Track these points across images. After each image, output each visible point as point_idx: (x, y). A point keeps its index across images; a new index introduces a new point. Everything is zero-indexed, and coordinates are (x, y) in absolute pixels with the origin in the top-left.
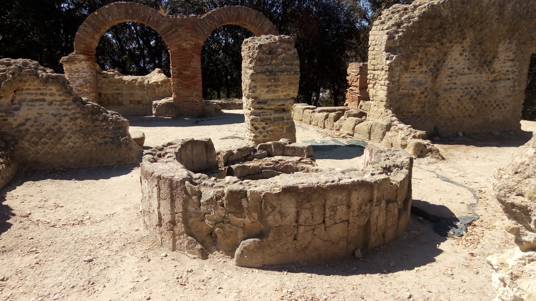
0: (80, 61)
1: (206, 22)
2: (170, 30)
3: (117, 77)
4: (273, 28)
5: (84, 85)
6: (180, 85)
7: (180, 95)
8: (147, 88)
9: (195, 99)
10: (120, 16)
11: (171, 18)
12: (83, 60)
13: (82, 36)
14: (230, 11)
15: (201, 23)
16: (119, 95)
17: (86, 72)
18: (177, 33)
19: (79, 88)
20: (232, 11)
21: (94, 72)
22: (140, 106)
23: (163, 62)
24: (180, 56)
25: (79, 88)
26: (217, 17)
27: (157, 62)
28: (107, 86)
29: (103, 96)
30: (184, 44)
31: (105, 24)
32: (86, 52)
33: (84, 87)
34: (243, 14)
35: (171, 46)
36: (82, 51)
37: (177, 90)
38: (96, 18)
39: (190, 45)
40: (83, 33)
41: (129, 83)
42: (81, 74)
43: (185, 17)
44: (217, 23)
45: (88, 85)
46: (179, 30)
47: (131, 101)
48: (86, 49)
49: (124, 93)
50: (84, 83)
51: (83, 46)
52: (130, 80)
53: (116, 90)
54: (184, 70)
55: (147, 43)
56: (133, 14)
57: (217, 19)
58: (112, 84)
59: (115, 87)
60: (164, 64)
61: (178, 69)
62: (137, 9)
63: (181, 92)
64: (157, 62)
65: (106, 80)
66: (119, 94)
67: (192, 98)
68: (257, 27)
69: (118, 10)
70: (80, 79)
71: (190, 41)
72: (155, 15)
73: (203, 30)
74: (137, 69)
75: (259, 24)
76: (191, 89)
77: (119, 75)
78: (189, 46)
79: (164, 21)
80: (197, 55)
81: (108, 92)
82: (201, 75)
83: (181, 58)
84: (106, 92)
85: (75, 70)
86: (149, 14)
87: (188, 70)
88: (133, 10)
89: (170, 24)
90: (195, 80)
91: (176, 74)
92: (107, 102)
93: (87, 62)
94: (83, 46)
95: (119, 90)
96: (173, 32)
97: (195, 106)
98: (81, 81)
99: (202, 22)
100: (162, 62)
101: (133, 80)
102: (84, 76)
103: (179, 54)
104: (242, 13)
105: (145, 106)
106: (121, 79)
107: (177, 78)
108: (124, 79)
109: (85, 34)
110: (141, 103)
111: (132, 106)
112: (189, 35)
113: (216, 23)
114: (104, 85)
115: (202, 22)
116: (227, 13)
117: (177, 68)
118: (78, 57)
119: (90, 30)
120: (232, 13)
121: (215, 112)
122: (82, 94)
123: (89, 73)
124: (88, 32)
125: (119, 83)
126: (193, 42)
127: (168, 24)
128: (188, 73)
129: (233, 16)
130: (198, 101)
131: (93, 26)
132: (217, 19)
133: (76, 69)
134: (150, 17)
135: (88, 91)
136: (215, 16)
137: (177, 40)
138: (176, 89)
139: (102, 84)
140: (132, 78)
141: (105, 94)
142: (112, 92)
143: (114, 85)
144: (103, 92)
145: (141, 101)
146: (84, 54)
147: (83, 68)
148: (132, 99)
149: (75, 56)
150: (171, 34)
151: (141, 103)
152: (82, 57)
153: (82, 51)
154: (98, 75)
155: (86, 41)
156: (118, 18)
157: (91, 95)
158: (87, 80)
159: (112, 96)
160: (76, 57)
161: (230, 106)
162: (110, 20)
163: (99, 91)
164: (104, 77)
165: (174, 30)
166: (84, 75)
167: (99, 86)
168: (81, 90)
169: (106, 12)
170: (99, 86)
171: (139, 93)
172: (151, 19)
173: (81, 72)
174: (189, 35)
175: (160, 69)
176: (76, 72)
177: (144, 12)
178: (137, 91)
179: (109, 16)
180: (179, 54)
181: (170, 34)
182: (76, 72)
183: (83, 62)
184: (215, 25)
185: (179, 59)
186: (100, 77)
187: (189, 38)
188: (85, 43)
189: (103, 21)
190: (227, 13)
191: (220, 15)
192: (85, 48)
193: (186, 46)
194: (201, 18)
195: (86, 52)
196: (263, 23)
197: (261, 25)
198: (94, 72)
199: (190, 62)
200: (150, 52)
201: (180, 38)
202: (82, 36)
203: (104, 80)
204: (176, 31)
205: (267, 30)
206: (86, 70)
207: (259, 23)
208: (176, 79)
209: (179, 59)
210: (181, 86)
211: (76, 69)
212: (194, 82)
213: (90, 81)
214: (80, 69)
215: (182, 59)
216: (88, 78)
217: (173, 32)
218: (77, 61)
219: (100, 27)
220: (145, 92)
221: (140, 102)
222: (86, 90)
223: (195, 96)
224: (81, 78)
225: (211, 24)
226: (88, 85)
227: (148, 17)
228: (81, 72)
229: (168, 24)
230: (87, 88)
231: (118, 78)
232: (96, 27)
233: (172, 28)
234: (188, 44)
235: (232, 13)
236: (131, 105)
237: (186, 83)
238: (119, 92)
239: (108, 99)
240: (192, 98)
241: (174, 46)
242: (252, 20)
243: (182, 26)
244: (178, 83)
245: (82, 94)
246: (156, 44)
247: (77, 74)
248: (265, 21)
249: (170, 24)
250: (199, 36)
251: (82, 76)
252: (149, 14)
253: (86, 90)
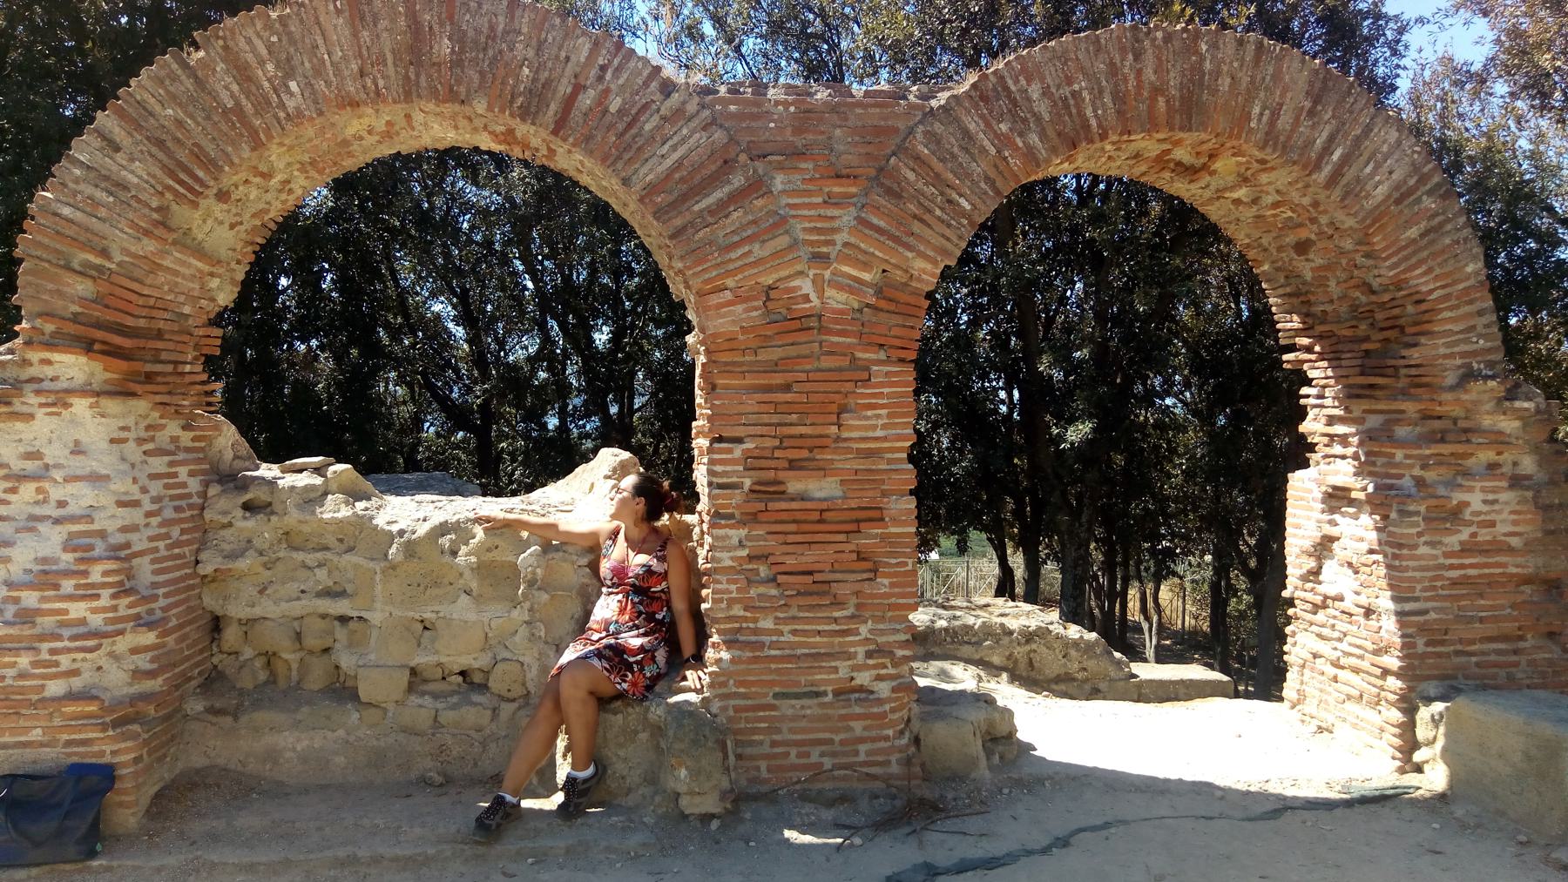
0: (60, 399)
1: (966, 133)
2: (714, 180)
3: (335, 509)
4: (1423, 179)
5: (68, 574)
6: (764, 571)
7: (762, 645)
8: (531, 583)
9: (863, 678)
10: (362, 74)
11: (723, 101)
12: (84, 392)
13: (78, 216)
14: (1137, 57)
15: (933, 138)
16: (341, 633)
17: (95, 479)
18: (759, 203)
19: (30, 599)
20: (1149, 58)
21: (183, 471)
22: (473, 714)
23: (639, 409)
24: (775, 367)
25: (30, 599)
26: (1046, 93)
27: (614, 410)
28: (267, 566)
29: (231, 635)
30: (806, 286)
31: (254, 134)
32: (99, 334)
33: (68, 586)
34: (1225, 83)
35: (715, 299)
36: (71, 328)
37: (738, 611)
38: (189, 83)
39: (851, 291)
40: (89, 190)
41: (412, 548)
42: (56, 493)
43: (822, 94)
44: (1043, 135)
45: (96, 574)
46: (779, 182)
47: (414, 672)
48: (97, 313)
49: (376, 617)
50: (68, 557)
51: (82, 288)
52: (423, 529)
53: (328, 593)
54: (793, 465)
55: (580, 339)
56: (457, 62)
57: (1043, 108)
58: (299, 556)
59: (321, 574)
60: (640, 418)
61: (752, 462)
62: (492, 28)
63: (767, 623)
64: (614, 410)
65: (260, 529)
66: (344, 619)
67: (844, 669)
68: (1317, 167)
69: (355, 35)
70: (44, 528)
71: (847, 259)
72: (618, 70)
73: (938, 180)
74: (1536, 225)
75: (1327, 150)
76: (838, 603)
77: (355, 496)
78: (837, 299)
79: (679, 113)
80: (888, 361)
81: (267, 608)
82: (911, 503)
83: (778, 379)
84: (258, 611)
85: (17, 465)
86: (570, 69)
87: (824, 470)
88: (459, 37)
89: (719, 135)
90: (869, 538)
91: (737, 497)
92: (263, 676)
93: (112, 405)
94: (82, 288)
95: (342, 594)
96: (736, 198)
97: (858, 727)
98: (51, 542)
99: (938, 128)
100: (632, 412)
101: (443, 529)
102: (73, 509)
103: (763, 356)
104: (1217, 74)
105: (507, 709)
106: (363, 524)
107: (742, 524)
108: (380, 521)
109: (97, 204)
110: (483, 687)
111: (421, 710)
112: (846, 217)
113: (1034, 139)
114: (242, 564)
115: (938, 128)
116: (1113, 70)
117: (748, 456)
118: (49, 371)
119: (138, 172)
120: (1149, 74)
121: (989, 754)
122: (42, 638)
123: (122, 486)
124: (124, 187)
125: (350, 550)
126: (866, 266)
127: (700, 138)
128: (823, 488)
129: (1157, 91)
130: (884, 689)
131: (160, 144)
132: (1043, 108)
133: (29, 456)
134: (578, 88)
135: (96, 621)
136: (1035, 91)
137: (758, 251)
138: (731, 602)
139: (234, 556)
140: (437, 518)
141: (251, 622)
142: (297, 608)
143: (311, 558)
144: (237, 610)
145: (486, 673)
146: (87, 347)
147: (78, 450)
148: (421, 659)
149: (25, 363)
150: (721, 209)
151: (483, 687)
152: (72, 366)
153: (71, 328)
154: (214, 490)
155: (104, 253)
156: (351, 87)
157: (122, 644)
158: (102, 534)
159: (298, 636)
160: (33, 371)
161: (978, 644)
162: (291, 104)
163: (210, 601)
164: (248, 507)
165: (738, 181)
166: (82, 497)
167: (207, 569)
168: (38, 612)
169: (270, 47)
170: (207, 569)
171: (472, 616)
172: (587, 100)
173: (58, 475)
174: (846, 217)
175: (626, 455)
176: (23, 477)
177: (539, 50)
178: (462, 609)
179: (289, 74)
180: (763, 356)
181: (711, 211)
182: (23, 477)
183: (81, 405)
184: (1030, 155)
185: (768, 389)
186: (224, 506)
187: (840, 238)
188: (100, 269)
189: (238, 109)
190: (1113, 70)
191: (1069, 81)
192: (98, 300)
193: (815, 301)
194: (934, 103)
195: (99, 334)
196: (1358, 141)
197: (1346, 160)
198: (183, 471)
199: (843, 409)
200: (586, 371)
201: (783, 241)
202: (78, 216)
203: (250, 524)
204: (757, 186)
205: (1381, 191)
206: (102, 460)
207: (1331, 139)
208: (736, 534)
209: (768, 389)
210: (773, 580)
211: (29, 456)
212: (861, 556)
213: (120, 538)
214: (54, 453)
215: (787, 388)
216: (111, 520)
217: (736, 198)
218: (34, 400)
219: (210, 149)
220: (519, 615)
221: (477, 678)
222: (77, 610)
223: (861, 650)
224: (57, 521)
225: (1003, 141)
226: (96, 574)
227: (564, 88)
228: (58, 475)
229: (700, 138)
230: (88, 593)
231: (345, 512)
232: (183, 155)
233: (728, 164)
234: (833, 284)
235: (1149, 74)
236: (414, 700)
237: (809, 558)
238: (342, 607)
239: (269, 658)
240: (844, 669)
241: (739, 299)
242: (1284, 122)
243: (800, 154)
244: (751, 558)
245: (42, 638)
246: (616, 338)
247: (28, 491)
248: (1368, 130)
249: (719, 135)
250: (917, 227)
251: (62, 504)
252: (570, 69)
253: (77, 610)
